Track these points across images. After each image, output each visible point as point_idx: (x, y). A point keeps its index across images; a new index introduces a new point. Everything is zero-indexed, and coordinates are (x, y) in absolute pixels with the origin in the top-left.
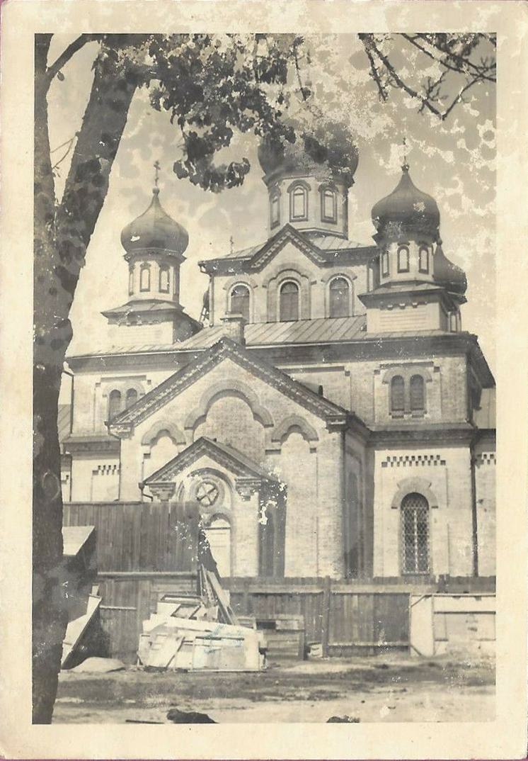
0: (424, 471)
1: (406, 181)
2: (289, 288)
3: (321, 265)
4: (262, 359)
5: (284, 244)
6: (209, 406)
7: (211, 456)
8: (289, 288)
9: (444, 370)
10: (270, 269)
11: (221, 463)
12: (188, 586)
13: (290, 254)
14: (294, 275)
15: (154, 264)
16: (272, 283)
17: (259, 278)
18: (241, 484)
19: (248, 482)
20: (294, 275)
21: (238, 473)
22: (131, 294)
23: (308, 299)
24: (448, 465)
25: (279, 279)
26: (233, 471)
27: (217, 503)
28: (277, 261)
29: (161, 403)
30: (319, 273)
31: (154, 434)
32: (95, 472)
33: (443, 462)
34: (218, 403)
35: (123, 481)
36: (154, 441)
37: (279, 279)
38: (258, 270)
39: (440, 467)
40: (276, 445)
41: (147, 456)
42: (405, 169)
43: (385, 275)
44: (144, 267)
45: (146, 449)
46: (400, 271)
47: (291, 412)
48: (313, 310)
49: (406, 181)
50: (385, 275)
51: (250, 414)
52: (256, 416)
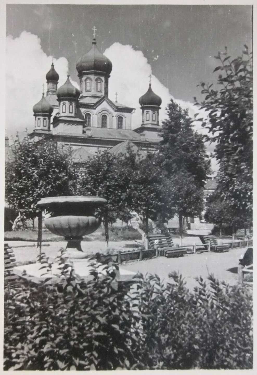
1: (150, 90)
2: (104, 118)
3: (116, 111)
8: (104, 118)
20: (107, 113)
30: (115, 114)
38: (95, 109)
42: (150, 85)
49: (150, 90)
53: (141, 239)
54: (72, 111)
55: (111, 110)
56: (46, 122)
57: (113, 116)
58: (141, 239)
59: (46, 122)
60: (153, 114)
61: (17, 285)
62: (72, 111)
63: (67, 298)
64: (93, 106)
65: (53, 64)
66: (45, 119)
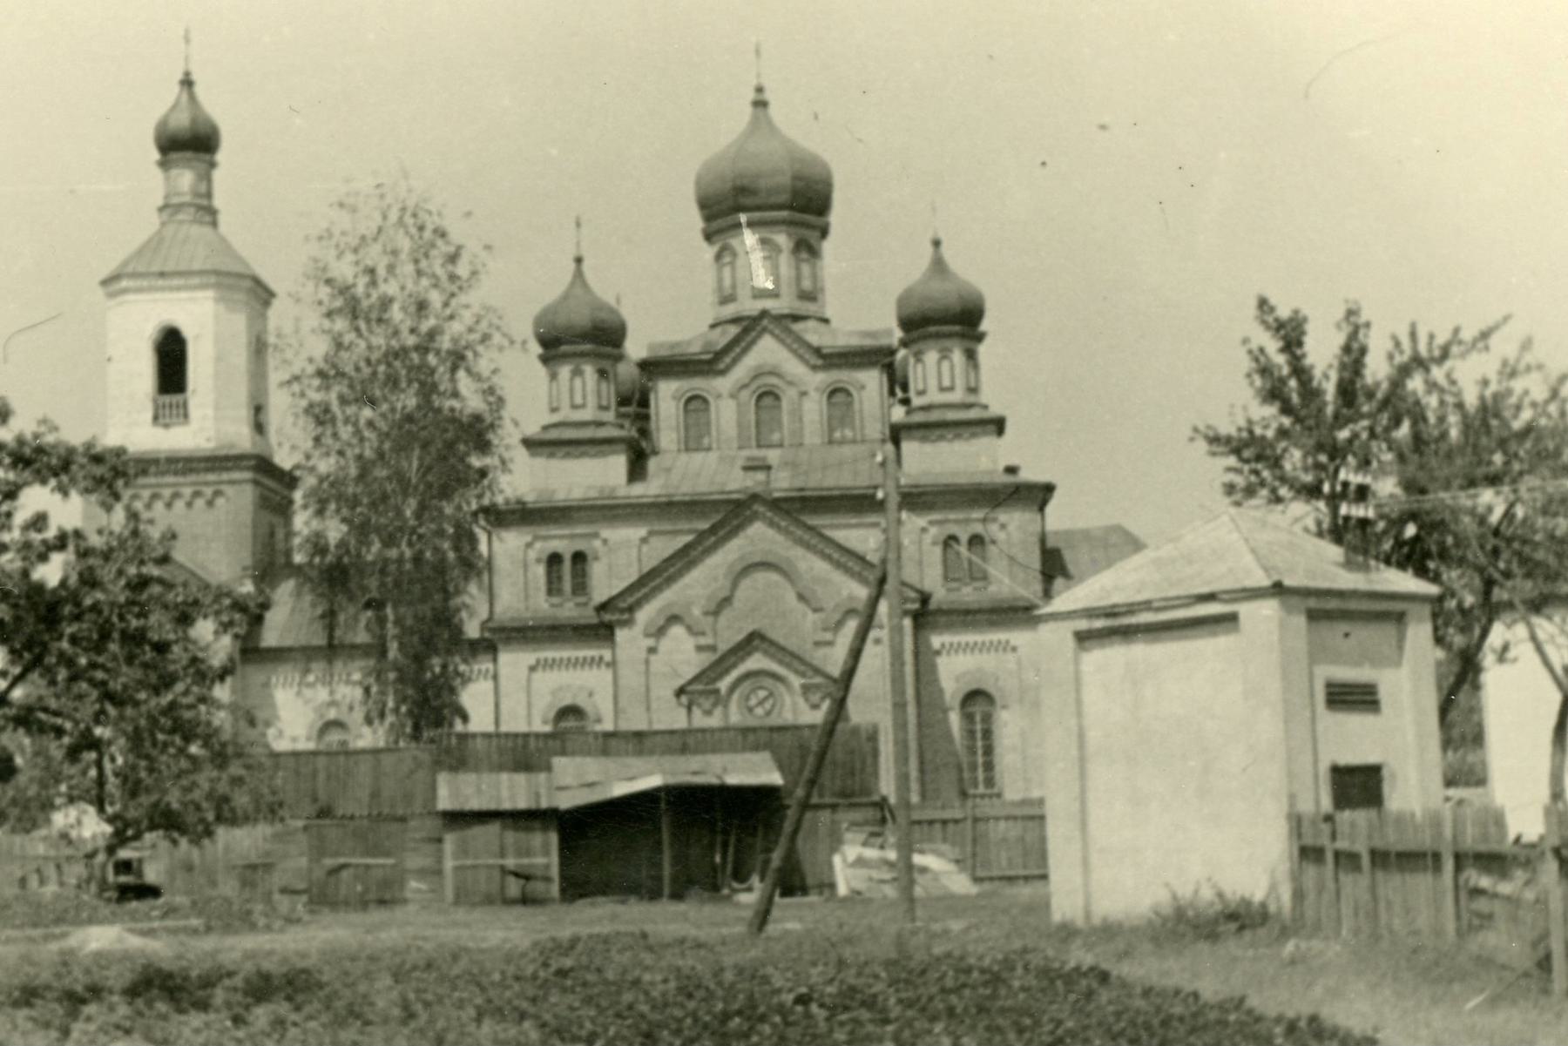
0: (988, 661)
2: (767, 397)
3: (814, 368)
4: (788, 513)
5: (759, 336)
6: (735, 585)
7: (766, 653)
8: (767, 397)
9: (1011, 528)
10: (741, 372)
11: (781, 662)
12: (871, 813)
13: (767, 350)
14: (774, 380)
15: (589, 370)
16: (745, 394)
17: (723, 384)
18: (806, 689)
19: (817, 687)
20: (774, 380)
21: (803, 675)
22: (554, 410)
23: (798, 415)
24: (1021, 651)
25: (753, 386)
26: (797, 672)
27: (776, 711)
28: (750, 361)
29: (670, 580)
30: (818, 380)
31: (661, 622)
32: (532, 669)
33: (1014, 649)
34: (746, 583)
35: (622, 682)
36: (660, 632)
37: (753, 386)
38: (723, 373)
39: (1010, 656)
40: (828, 636)
41: (652, 650)
43: (921, 393)
44: (577, 372)
45: (651, 642)
46: (942, 389)
47: (845, 593)
48: (807, 432)
50: (921, 393)
51: (791, 597)
52: (801, 597)
53: (1330, 685)
54: (584, 397)
55: (794, 367)
56: (952, 368)
57: (804, 394)
58: (1330, 685)
59: (952, 368)
60: (944, 357)
61: (241, 469)
62: (584, 397)
63: (650, 773)
64: (709, 362)
65: (187, 74)
66: (577, 372)
